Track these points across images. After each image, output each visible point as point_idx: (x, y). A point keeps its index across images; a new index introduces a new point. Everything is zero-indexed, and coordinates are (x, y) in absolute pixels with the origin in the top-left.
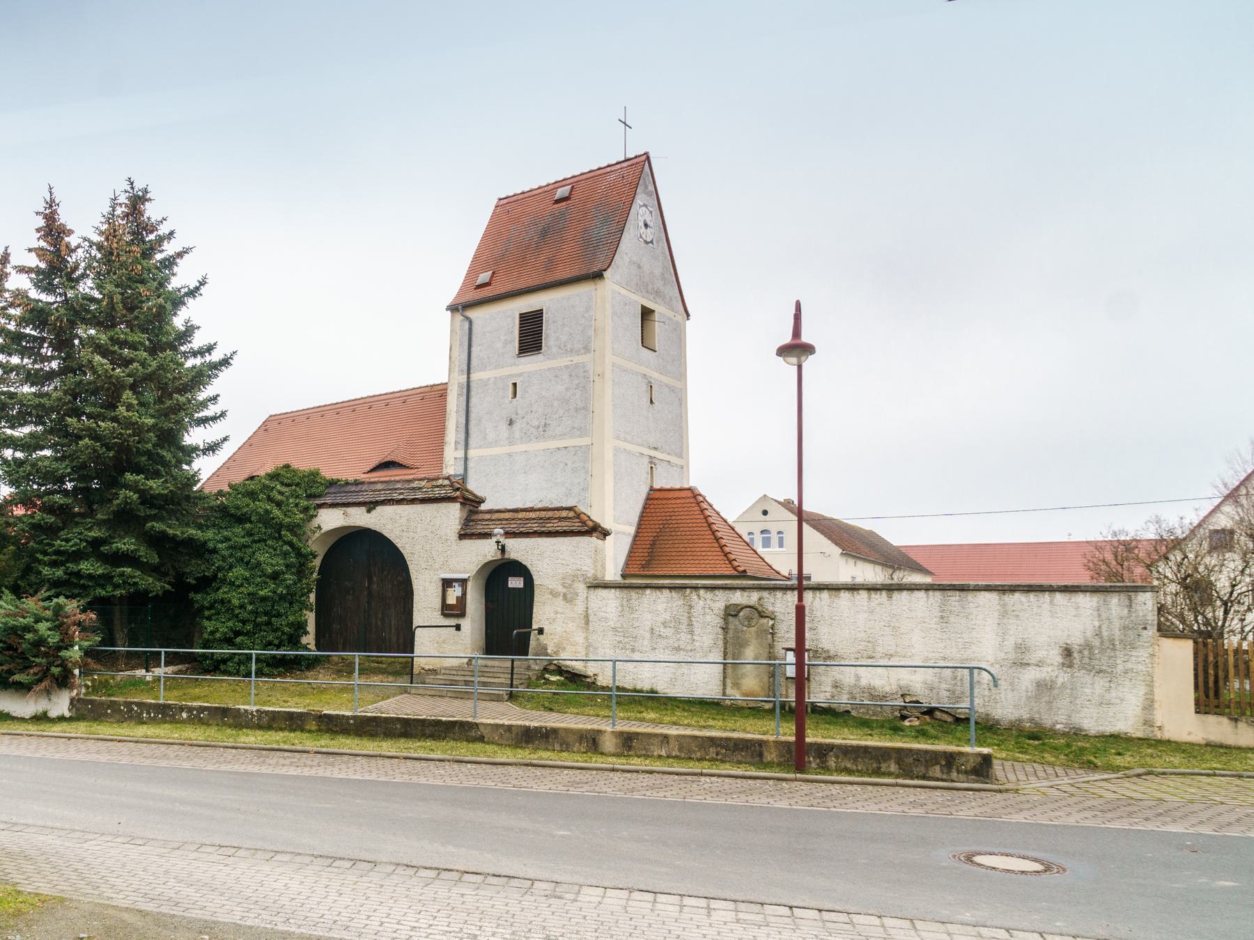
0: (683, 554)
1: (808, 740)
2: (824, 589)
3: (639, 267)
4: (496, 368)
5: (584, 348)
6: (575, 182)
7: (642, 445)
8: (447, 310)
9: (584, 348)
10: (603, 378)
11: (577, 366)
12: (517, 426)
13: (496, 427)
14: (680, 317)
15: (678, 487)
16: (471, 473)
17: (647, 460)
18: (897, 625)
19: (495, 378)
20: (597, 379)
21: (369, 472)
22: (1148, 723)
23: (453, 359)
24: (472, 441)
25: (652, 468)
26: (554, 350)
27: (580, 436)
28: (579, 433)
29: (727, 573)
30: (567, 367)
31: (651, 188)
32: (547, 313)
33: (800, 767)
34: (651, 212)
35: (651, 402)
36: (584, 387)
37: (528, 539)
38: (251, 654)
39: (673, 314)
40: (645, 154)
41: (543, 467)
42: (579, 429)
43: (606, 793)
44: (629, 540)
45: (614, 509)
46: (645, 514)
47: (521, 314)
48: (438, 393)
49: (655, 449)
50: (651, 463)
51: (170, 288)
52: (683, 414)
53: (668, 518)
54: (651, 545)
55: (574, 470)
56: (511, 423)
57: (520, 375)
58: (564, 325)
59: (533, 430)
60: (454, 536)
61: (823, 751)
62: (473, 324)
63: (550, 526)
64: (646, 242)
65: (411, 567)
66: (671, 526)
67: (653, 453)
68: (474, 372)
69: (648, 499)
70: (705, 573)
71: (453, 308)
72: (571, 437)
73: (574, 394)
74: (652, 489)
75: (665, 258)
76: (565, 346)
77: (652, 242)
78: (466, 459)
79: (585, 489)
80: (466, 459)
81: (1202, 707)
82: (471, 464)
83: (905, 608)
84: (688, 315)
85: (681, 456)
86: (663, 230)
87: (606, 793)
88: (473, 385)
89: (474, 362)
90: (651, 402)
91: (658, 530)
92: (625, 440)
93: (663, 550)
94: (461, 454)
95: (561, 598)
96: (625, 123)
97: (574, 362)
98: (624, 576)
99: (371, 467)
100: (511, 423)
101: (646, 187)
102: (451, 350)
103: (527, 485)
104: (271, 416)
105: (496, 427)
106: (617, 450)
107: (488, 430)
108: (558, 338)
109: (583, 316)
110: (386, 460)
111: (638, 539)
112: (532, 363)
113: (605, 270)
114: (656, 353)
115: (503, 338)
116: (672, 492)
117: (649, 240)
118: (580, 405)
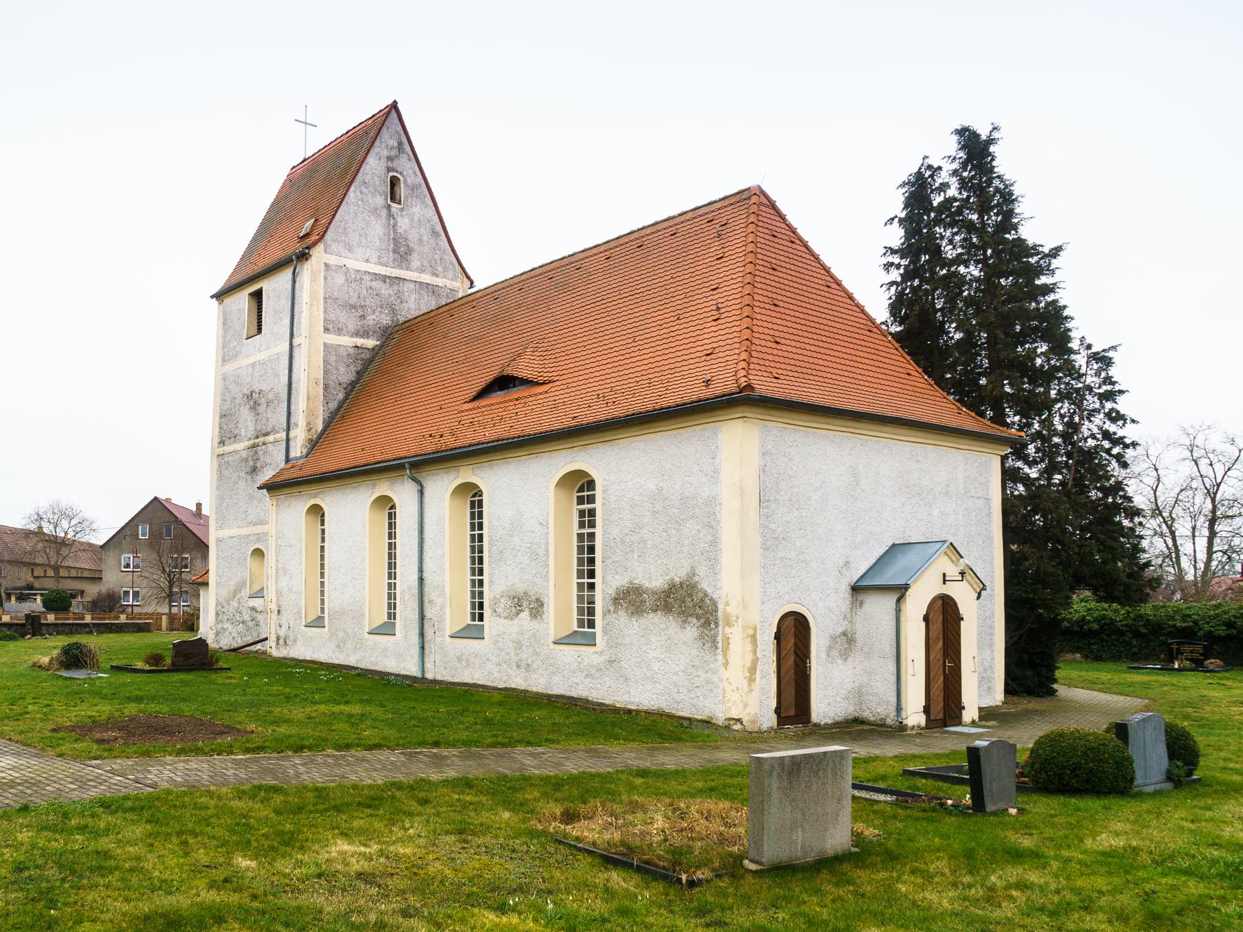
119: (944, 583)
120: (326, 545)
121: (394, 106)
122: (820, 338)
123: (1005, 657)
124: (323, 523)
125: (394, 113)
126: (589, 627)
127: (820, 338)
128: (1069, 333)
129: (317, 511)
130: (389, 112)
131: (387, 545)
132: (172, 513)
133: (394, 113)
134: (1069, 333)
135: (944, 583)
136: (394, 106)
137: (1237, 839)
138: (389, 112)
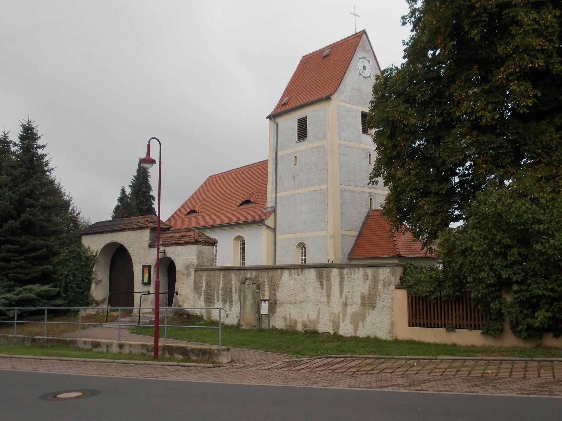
1: (159, 344)
2: (230, 270)
3: (359, 91)
5: (324, 137)
8: (267, 118)
9: (324, 137)
16: (278, 205)
17: (367, 195)
18: (304, 286)
21: (239, 206)
22: (391, 332)
25: (371, 199)
30: (317, 147)
31: (368, 48)
32: (308, 119)
33: (156, 357)
34: (369, 61)
37: (173, 247)
38: (45, 309)
40: (363, 30)
43: (556, 389)
44: (355, 239)
45: (341, 223)
47: (298, 119)
48: (264, 164)
51: (400, 69)
57: (298, 152)
60: (147, 246)
61: (171, 350)
62: (279, 126)
63: (182, 240)
64: (366, 78)
65: (133, 262)
69: (368, 216)
71: (269, 117)
74: (371, 210)
76: (316, 136)
77: (369, 77)
78: (276, 198)
80: (276, 198)
81: (413, 323)
82: (278, 201)
83: (307, 277)
87: (556, 389)
88: (279, 158)
89: (279, 146)
94: (273, 195)
95: (185, 276)
96: (355, 14)
98: (350, 259)
99: (240, 203)
101: (364, 48)
103: (301, 211)
104: (210, 176)
110: (246, 200)
112: (303, 146)
113: (331, 95)
117: (366, 76)
125: (364, 35)
130: (362, 34)
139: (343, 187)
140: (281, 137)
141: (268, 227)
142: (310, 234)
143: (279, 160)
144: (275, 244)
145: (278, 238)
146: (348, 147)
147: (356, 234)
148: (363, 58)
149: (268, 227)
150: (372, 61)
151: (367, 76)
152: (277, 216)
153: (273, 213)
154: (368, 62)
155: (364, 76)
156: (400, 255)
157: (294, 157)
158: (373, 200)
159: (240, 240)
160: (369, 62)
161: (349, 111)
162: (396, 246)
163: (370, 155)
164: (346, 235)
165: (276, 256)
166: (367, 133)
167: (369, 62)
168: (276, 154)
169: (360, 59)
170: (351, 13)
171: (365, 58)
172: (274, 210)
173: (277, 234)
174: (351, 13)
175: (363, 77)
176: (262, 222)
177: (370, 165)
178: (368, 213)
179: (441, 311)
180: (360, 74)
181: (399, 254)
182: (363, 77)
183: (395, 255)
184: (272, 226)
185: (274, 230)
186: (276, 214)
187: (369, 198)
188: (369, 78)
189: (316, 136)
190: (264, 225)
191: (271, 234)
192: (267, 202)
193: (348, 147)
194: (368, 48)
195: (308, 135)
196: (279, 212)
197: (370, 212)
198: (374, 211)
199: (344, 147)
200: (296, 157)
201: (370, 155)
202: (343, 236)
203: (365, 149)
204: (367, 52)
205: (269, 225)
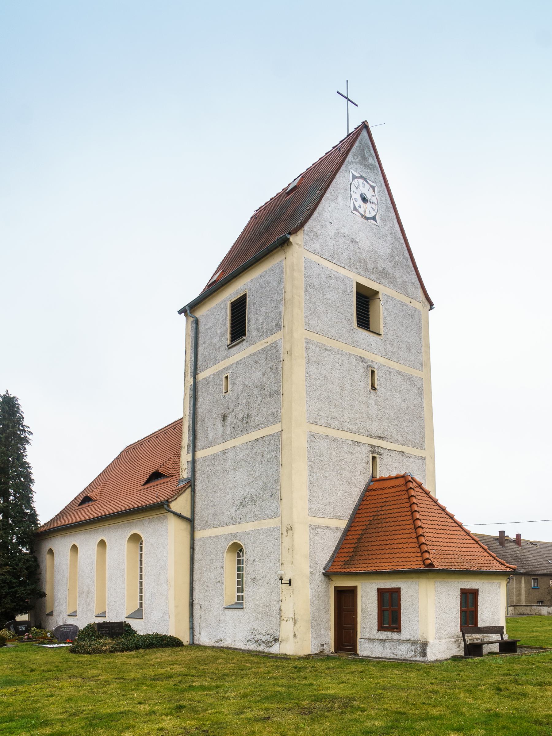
0: (383, 547)
3: (353, 241)
4: (214, 364)
6: (303, 176)
7: (358, 433)
8: (180, 312)
10: (291, 354)
11: (271, 347)
12: (229, 420)
13: (214, 425)
14: (419, 305)
15: (386, 476)
16: (198, 474)
17: (365, 450)
19: (214, 374)
20: (286, 357)
23: (187, 363)
24: (199, 444)
25: (374, 458)
26: (254, 333)
27: (273, 424)
28: (272, 420)
29: (415, 568)
34: (373, 188)
35: (373, 387)
36: (276, 369)
39: (409, 299)
41: (246, 461)
42: (272, 415)
44: (339, 535)
45: (310, 501)
46: (361, 507)
49: (381, 438)
50: (373, 452)
52: (425, 405)
53: (380, 509)
54: (358, 539)
55: (269, 461)
56: (224, 418)
57: (230, 367)
58: (261, 305)
59: (239, 423)
64: (367, 218)
66: (380, 517)
67: (376, 442)
68: (201, 372)
69: (368, 490)
70: (396, 569)
71: (183, 311)
72: (267, 426)
73: (269, 379)
74: (373, 479)
75: (397, 240)
76: (262, 327)
77: (374, 218)
79: (277, 481)
82: (198, 466)
84: (431, 304)
85: (421, 447)
86: (392, 210)
88: (199, 385)
89: (200, 363)
90: (373, 387)
91: (368, 523)
92: (328, 426)
93: (370, 544)
96: (347, 98)
97: (269, 344)
100: (224, 418)
101: (365, 159)
102: (185, 353)
104: (127, 447)
105: (214, 425)
106: (312, 437)
107: (209, 429)
108: (257, 320)
109: (276, 291)
111: (349, 533)
114: (381, 337)
115: (219, 332)
116: (389, 481)
117: (368, 215)
118: (274, 388)
119: (290, 580)
120: (143, 581)
121: (365, 126)
122: (136, 475)
123: (357, 620)
124: (141, 550)
125: (364, 133)
126: (352, 643)
127: (136, 475)
128: (37, 517)
129: (136, 539)
130: (361, 130)
131: (139, 583)
132: (372, 467)
133: (364, 133)
134: (37, 517)
135: (290, 580)
136: (365, 126)
137: (432, 714)
138: (361, 130)
139: (316, 429)
140: (204, 343)
141: (179, 516)
142: (249, 527)
143: (200, 390)
144: (192, 548)
145: (198, 535)
146: (326, 350)
147: (343, 524)
148: (361, 177)
149: (179, 516)
150: (380, 189)
151: (370, 216)
152: (198, 495)
153: (189, 490)
154: (371, 190)
155: (363, 214)
156: (433, 566)
157: (224, 379)
158: (378, 460)
159: (136, 539)
160: (374, 191)
161: (330, 278)
162: (425, 548)
163: (373, 372)
164: (319, 527)
165: (195, 571)
166: (369, 328)
167: (374, 191)
168: (195, 378)
169: (354, 177)
170: (338, 92)
171: (365, 179)
172: (191, 484)
173: (195, 530)
174: (338, 92)
175: (362, 215)
176: (163, 507)
177: (373, 392)
178: (368, 485)
179: (239, 327)
180: (355, 209)
181: (431, 565)
182: (362, 215)
183: (422, 567)
184: (188, 514)
185: (191, 521)
186: (194, 491)
187: (371, 455)
188: (373, 222)
189: (262, 327)
190: (170, 511)
191: (184, 527)
192: (181, 471)
193: (326, 350)
194: (372, 161)
195: (248, 328)
196: (199, 487)
197: (371, 484)
198: (380, 480)
199: (318, 348)
200: (227, 377)
201: (373, 372)
202: (313, 528)
203: (362, 359)
204: (372, 168)
205: (178, 512)
